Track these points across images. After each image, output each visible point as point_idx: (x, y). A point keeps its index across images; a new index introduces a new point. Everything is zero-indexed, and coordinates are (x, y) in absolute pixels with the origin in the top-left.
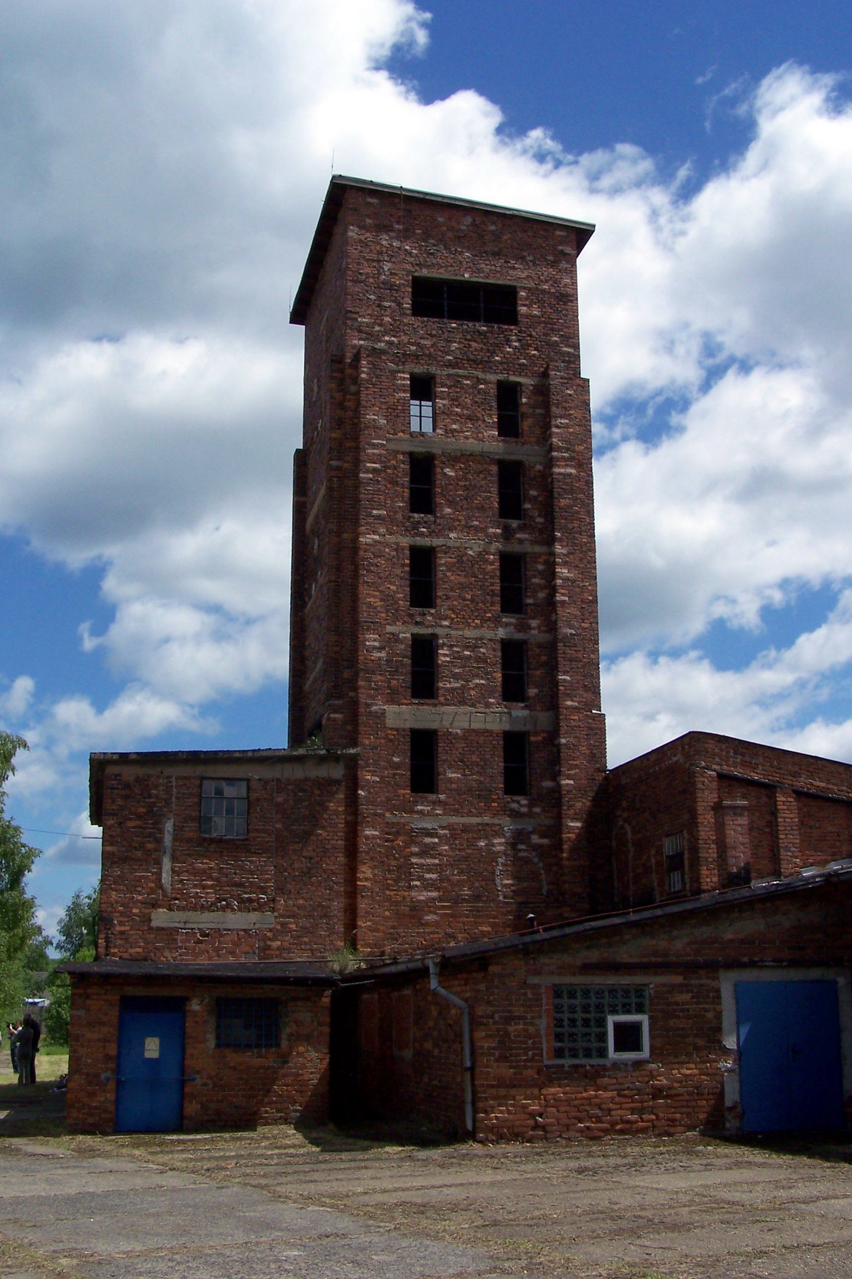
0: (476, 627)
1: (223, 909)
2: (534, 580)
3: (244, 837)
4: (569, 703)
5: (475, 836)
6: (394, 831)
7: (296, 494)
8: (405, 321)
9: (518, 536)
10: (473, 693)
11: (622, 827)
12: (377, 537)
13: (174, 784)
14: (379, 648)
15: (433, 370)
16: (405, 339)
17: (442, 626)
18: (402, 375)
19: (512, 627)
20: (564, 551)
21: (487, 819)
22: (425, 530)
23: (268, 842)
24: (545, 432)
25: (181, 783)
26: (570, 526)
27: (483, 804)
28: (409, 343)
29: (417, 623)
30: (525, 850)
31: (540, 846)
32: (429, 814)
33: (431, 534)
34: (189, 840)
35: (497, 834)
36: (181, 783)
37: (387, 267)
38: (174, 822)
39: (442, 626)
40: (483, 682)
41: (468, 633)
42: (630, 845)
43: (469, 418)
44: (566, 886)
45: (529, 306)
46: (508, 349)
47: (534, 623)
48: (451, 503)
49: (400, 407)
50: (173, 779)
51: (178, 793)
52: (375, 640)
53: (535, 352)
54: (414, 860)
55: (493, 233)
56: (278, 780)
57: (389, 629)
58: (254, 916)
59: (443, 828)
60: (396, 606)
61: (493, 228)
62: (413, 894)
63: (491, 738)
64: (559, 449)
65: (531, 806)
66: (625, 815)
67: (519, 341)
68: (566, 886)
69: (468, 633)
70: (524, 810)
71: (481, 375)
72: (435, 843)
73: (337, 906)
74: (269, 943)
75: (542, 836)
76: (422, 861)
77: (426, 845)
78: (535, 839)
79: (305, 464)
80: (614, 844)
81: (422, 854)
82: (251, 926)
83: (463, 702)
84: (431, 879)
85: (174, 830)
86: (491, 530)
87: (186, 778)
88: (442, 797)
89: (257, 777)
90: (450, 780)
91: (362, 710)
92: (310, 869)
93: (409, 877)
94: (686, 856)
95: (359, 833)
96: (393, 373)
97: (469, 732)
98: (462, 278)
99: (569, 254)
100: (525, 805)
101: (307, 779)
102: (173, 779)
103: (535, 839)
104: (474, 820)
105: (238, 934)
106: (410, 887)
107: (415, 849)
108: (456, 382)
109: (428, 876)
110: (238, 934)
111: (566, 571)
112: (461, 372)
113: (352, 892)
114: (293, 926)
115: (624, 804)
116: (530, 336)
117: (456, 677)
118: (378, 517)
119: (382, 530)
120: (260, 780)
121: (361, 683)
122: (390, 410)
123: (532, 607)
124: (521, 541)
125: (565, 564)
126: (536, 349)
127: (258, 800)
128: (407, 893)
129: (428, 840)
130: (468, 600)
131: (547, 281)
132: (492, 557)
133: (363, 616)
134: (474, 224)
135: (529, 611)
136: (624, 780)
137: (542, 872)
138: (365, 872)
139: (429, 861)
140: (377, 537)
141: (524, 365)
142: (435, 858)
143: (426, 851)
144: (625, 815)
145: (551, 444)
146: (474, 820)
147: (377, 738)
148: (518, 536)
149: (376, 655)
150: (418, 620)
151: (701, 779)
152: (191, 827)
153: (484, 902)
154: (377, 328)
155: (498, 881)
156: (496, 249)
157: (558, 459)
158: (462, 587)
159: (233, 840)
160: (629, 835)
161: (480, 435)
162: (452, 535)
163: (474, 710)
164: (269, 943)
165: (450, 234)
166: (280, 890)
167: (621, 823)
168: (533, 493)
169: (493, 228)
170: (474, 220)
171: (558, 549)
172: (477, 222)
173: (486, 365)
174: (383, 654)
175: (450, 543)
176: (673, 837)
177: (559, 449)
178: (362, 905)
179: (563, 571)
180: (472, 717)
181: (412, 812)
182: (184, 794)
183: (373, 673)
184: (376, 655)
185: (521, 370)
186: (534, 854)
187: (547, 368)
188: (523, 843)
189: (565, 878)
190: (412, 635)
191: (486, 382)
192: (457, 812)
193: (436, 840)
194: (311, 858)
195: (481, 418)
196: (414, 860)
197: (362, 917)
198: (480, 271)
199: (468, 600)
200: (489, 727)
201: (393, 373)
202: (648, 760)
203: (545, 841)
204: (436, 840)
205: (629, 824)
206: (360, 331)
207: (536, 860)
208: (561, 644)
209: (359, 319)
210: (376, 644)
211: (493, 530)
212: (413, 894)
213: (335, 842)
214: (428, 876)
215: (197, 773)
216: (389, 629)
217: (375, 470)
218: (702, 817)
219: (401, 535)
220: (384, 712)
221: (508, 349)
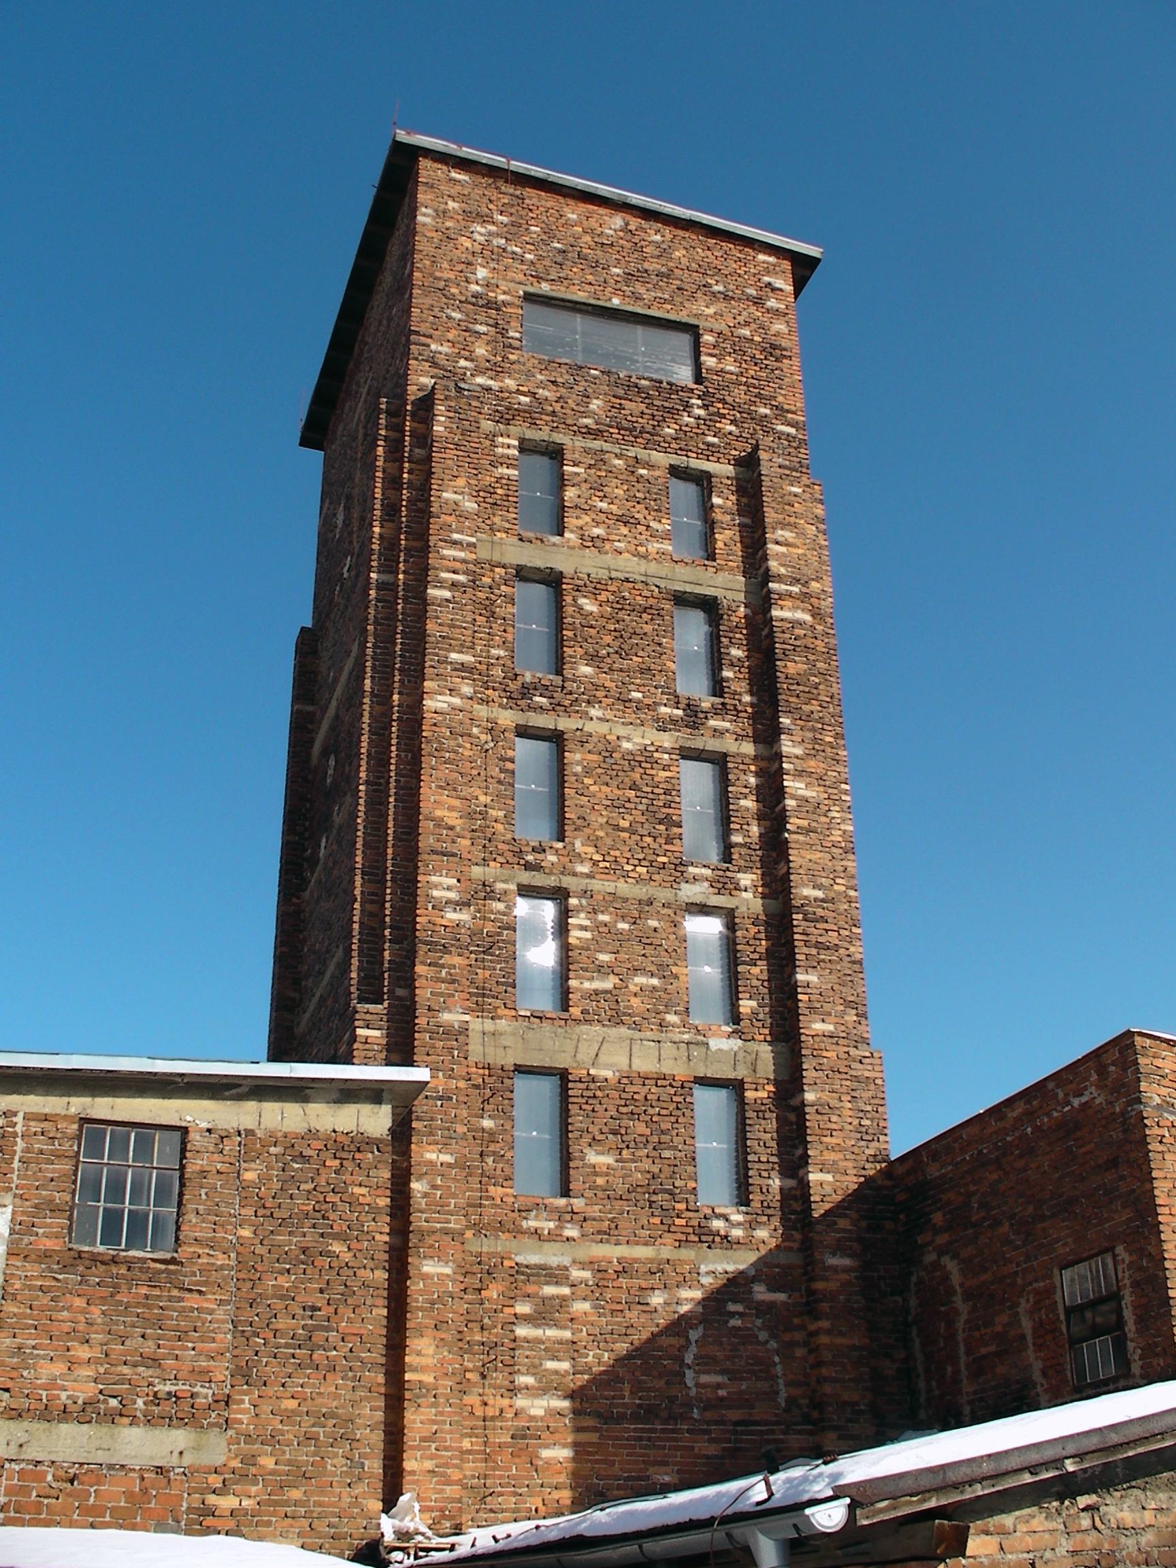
0: (639, 880)
1: (112, 1418)
2: (743, 802)
3: (168, 1256)
4: (818, 1026)
5: (644, 1284)
6: (479, 1272)
7: (296, 698)
8: (511, 357)
9: (712, 723)
10: (635, 1002)
11: (936, 1265)
12: (456, 701)
13: (19, 1129)
14: (457, 903)
15: (559, 438)
16: (510, 383)
17: (575, 874)
18: (506, 441)
19: (706, 884)
20: (799, 751)
21: (666, 1252)
22: (544, 700)
23: (222, 1268)
24: (754, 554)
25: (35, 1127)
26: (806, 708)
27: (657, 1220)
28: (518, 392)
29: (528, 867)
30: (741, 1315)
31: (771, 1305)
32: (554, 1237)
33: (556, 707)
34: (46, 1255)
35: (684, 1282)
36: (35, 1127)
37: (482, 273)
38: (14, 1213)
39: (575, 874)
40: (655, 982)
41: (623, 888)
42: (958, 1300)
43: (624, 520)
44: (828, 1389)
45: (720, 358)
46: (687, 419)
47: (746, 879)
48: (593, 658)
49: (499, 491)
50: (19, 1119)
51: (27, 1150)
52: (449, 888)
53: (733, 428)
54: (522, 1331)
55: (658, 245)
56: (250, 1132)
57: (477, 871)
58: (180, 1438)
59: (583, 1266)
60: (489, 832)
61: (658, 238)
62: (520, 1402)
63: (672, 1091)
64: (779, 578)
65: (751, 1225)
66: (941, 1239)
67: (705, 407)
68: (828, 1389)
69: (623, 888)
70: (737, 1233)
71: (642, 454)
72: (564, 1299)
73: (372, 1413)
74: (212, 1499)
75: (771, 1289)
76: (538, 1333)
77: (544, 1300)
78: (761, 1292)
79: (315, 653)
80: (913, 1302)
81: (537, 1319)
82: (175, 1460)
83: (617, 1019)
84: (557, 1372)
85: (12, 1232)
86: (663, 710)
87: (46, 1118)
88: (578, 1203)
89: (204, 1125)
90: (594, 1171)
91: (421, 1021)
92: (311, 1330)
93: (511, 1368)
94: (1128, 1299)
95: (412, 1272)
96: (491, 437)
97: (628, 1078)
98: (608, 305)
99: (781, 290)
100: (739, 1224)
101: (311, 1134)
102: (19, 1119)
103: (761, 1292)
104: (642, 1252)
105: (143, 1479)
106: (513, 1390)
107: (523, 1308)
108: (599, 460)
109: (550, 1365)
110: (143, 1479)
111: (803, 786)
112: (607, 446)
113: (396, 1397)
114: (268, 1462)
115: (938, 1218)
116: (723, 401)
117: (602, 970)
118: (463, 667)
119: (467, 690)
120: (209, 1130)
121: (420, 969)
122: (481, 494)
123: (744, 851)
124: (718, 733)
125: (800, 774)
126: (733, 422)
127: (203, 1173)
128: (506, 1402)
129: (549, 1290)
130: (623, 830)
131: (747, 324)
132: (666, 756)
133: (427, 841)
134: (625, 229)
135: (735, 856)
136: (934, 1171)
137: (777, 1359)
138: (425, 1355)
139: (551, 1333)
140: (456, 701)
141: (713, 445)
142: (564, 1328)
143: (545, 1313)
144: (941, 1239)
145: (768, 569)
146: (642, 1252)
147: (450, 1077)
148: (712, 723)
149: (452, 916)
150: (530, 858)
151: (1156, 1131)
152: (49, 1226)
153: (665, 1421)
154: (463, 363)
155: (689, 1374)
156: (664, 269)
157: (781, 596)
158: (615, 805)
159: (144, 1260)
160: (956, 1278)
161: (642, 549)
162: (595, 712)
163: (637, 1035)
164: (212, 1499)
165: (587, 238)
166: (243, 1373)
167: (930, 1258)
168: (736, 652)
169: (658, 238)
170: (627, 224)
171: (788, 746)
172: (632, 227)
173: (653, 440)
174: (464, 916)
175: (589, 727)
176: (1086, 1263)
177: (779, 578)
178: (416, 1419)
179: (798, 785)
180: (635, 1048)
181: (518, 1232)
182: (41, 1152)
183: (445, 949)
184: (452, 916)
185: (710, 452)
186: (759, 1322)
187: (756, 448)
188: (735, 1302)
189: (824, 1371)
190: (518, 885)
191: (650, 466)
192: (607, 1235)
193: (566, 1291)
194: (314, 1309)
195: (643, 521)
196: (522, 1331)
197: (413, 1448)
198: (637, 298)
199: (623, 830)
200: (667, 1068)
201: (491, 437)
202: (1002, 1117)
203: (781, 1297)
204: (566, 1291)
205: (955, 1256)
206: (435, 365)
207: (763, 1336)
208: (800, 916)
209: (433, 347)
210: (452, 895)
211: (668, 710)
212: (520, 1402)
213: (368, 1273)
214: (550, 1365)
215: (73, 1110)
216: (477, 871)
217: (454, 585)
218: (1166, 1210)
219: (501, 706)
220: (464, 1030)
221: (687, 419)
